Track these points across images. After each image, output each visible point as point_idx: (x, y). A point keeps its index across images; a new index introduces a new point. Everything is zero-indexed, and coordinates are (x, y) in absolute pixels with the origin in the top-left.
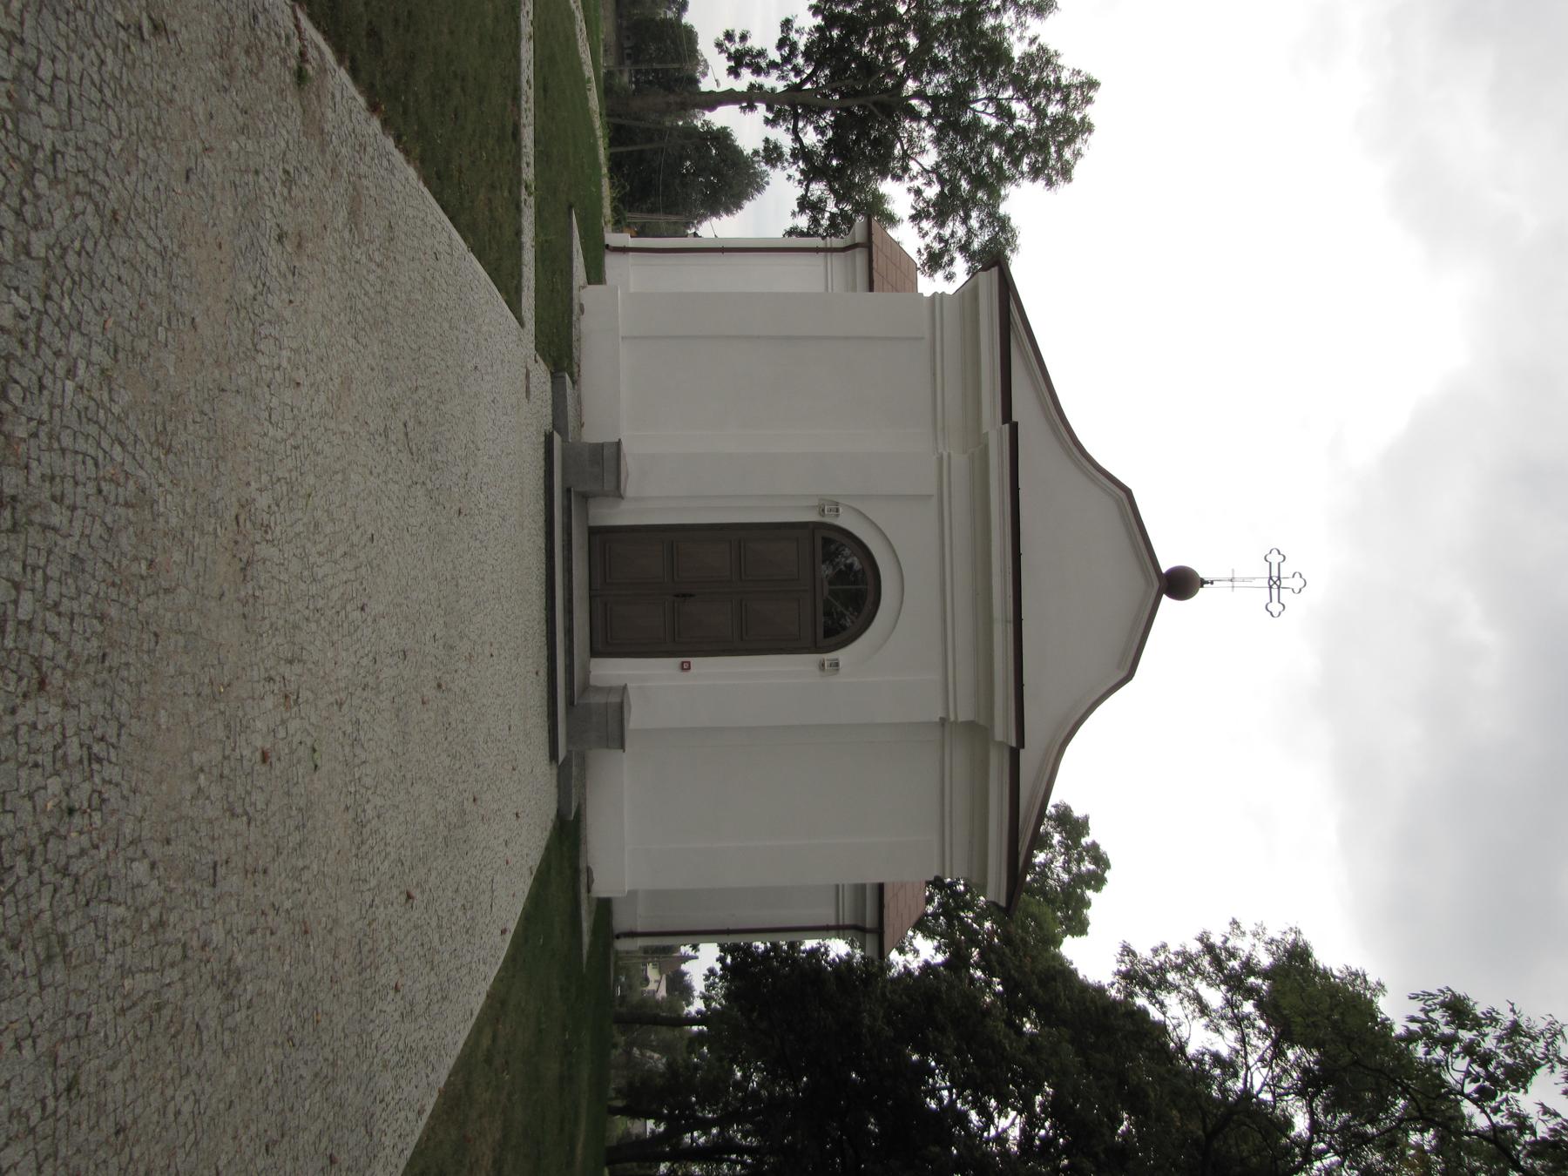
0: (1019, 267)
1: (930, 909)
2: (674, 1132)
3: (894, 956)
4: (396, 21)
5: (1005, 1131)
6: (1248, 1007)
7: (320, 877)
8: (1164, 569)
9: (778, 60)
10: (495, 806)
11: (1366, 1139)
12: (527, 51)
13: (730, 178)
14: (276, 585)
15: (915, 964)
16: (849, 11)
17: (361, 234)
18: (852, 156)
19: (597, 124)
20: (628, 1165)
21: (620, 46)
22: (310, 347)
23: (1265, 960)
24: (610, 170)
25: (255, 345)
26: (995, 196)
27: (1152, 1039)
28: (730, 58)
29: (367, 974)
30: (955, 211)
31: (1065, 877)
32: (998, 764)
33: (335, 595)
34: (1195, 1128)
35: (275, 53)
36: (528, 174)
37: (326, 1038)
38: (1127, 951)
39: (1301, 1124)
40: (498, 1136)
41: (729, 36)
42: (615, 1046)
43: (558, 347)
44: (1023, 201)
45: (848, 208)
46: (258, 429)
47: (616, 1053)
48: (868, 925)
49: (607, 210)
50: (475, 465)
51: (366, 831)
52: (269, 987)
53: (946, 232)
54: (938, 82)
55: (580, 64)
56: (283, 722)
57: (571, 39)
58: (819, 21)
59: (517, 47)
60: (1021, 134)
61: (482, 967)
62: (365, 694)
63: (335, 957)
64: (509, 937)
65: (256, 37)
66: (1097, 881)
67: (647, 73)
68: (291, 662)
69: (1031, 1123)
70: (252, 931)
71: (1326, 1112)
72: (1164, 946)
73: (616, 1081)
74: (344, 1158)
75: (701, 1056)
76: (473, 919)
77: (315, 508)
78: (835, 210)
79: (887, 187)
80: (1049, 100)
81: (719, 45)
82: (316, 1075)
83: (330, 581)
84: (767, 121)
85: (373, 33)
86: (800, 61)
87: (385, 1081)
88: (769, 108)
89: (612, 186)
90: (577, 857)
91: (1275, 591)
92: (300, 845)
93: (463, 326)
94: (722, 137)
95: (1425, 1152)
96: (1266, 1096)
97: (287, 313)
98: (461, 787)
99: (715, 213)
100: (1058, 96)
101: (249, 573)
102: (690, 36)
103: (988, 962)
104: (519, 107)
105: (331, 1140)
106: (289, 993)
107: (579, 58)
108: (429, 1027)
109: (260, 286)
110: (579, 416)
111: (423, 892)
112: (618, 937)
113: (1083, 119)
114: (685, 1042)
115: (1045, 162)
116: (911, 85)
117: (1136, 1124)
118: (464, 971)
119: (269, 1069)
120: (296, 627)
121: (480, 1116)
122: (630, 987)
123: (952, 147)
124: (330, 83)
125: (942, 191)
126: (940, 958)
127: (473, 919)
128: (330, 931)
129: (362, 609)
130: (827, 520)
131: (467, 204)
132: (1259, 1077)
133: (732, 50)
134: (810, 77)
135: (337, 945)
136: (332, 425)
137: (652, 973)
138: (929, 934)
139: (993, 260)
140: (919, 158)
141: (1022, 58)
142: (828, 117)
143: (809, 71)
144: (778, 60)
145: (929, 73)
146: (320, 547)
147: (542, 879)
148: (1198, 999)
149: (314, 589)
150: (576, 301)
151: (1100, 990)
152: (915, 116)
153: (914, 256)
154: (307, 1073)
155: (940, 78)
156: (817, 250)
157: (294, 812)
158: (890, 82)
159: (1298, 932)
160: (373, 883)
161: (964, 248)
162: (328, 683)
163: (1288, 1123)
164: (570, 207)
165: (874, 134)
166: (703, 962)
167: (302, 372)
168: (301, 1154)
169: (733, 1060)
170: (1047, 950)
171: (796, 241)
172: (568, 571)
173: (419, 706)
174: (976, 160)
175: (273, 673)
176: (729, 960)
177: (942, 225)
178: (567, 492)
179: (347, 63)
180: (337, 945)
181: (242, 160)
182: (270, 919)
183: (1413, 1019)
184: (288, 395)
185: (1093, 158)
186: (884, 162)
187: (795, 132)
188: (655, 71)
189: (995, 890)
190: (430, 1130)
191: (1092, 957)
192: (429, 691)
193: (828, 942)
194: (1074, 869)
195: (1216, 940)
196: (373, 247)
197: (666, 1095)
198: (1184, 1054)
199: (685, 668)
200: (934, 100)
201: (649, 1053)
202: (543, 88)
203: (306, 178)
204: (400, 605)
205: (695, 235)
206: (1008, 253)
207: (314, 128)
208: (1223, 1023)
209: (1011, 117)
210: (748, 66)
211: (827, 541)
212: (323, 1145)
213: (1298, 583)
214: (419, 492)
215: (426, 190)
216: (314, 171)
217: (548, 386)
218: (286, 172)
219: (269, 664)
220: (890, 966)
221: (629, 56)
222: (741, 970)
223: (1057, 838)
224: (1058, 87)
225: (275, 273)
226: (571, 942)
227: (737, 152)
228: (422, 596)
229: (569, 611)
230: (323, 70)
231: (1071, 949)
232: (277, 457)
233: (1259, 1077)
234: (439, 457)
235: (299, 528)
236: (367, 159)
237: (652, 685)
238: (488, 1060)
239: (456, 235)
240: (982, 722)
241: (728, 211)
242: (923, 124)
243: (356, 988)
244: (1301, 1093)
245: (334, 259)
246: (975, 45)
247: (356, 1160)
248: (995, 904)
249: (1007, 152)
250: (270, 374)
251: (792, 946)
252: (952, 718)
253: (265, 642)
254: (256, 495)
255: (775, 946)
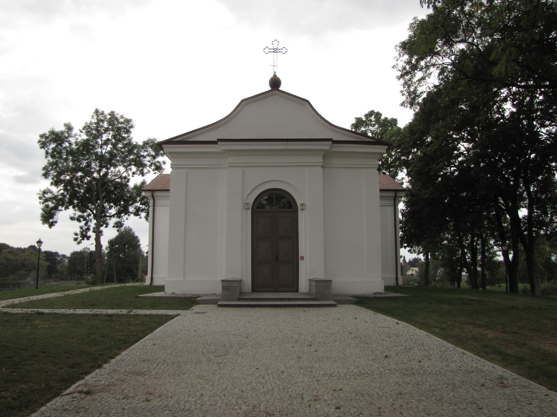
0: (161, 138)
1: (388, 174)
2: (467, 265)
3: (404, 186)
4: (68, 358)
5: (465, 148)
6: (423, 63)
7: (381, 388)
8: (270, 89)
9: (85, 222)
10: (353, 326)
11: (469, 23)
12: (80, 311)
13: (127, 240)
14: (275, 403)
15: (407, 179)
16: (68, 196)
17: (146, 371)
18: (122, 197)
19: (106, 287)
20: (478, 282)
21: (78, 279)
22: (188, 390)
23: (406, 57)
24: (123, 283)
25: (187, 410)
26: (136, 146)
27: (433, 97)
28: (83, 239)
29: (415, 372)
30: (140, 161)
31: (377, 126)
32: (338, 148)
33: (278, 382)
34: (464, 82)
35: (79, 402)
36: (124, 311)
37: (439, 387)
38: (403, 104)
39: (462, 46)
40: (471, 326)
41: (76, 239)
42: (435, 286)
43: (187, 302)
44: (138, 136)
45: (138, 199)
46: (218, 409)
47: (438, 285)
48: (394, 195)
49: (137, 284)
50: (230, 332)
51: (363, 372)
52: (421, 407)
53: (148, 164)
54: (95, 165)
55: (84, 293)
56: (325, 401)
57: (75, 296)
58: (71, 207)
59: (78, 315)
60: (114, 137)
61: (411, 331)
62: (314, 372)
63: (409, 383)
64: (399, 322)
65: (73, 409)
66: (378, 115)
67: (88, 270)
68: (303, 398)
69: (462, 139)
70: (401, 413)
71: (457, 37)
72: (401, 92)
73: (448, 285)
74: (482, 381)
75: (439, 255)
76: (393, 334)
77: (247, 389)
78: (139, 203)
79: (131, 184)
80: (102, 126)
81: (79, 243)
82: (452, 391)
83: (273, 384)
84: (107, 227)
85: (72, 366)
86: (85, 214)
87: (453, 366)
88: (102, 226)
89: (129, 282)
90: (370, 297)
91: (278, 51)
92: (369, 396)
93: (180, 335)
94: (112, 243)
95: (472, 4)
96: (453, 58)
97: (176, 398)
98: (346, 338)
99: (139, 246)
100: (101, 123)
101: (271, 413)
102: (75, 254)
103: (406, 153)
104: (100, 315)
105: (476, 386)
106: (423, 400)
107: (82, 293)
108: (433, 350)
109: (166, 408)
110: (211, 295)
111: (385, 352)
112: (398, 284)
113: (109, 115)
114: (434, 261)
115: (124, 128)
116: (95, 175)
117: (463, 102)
118: (412, 338)
119: (451, 408)
120: (290, 396)
121: (464, 332)
122: (414, 280)
123: (118, 161)
124: (90, 382)
125: (134, 165)
126: (405, 170)
127: (393, 334)
128: (400, 385)
129: (283, 372)
130: (251, 207)
131: (135, 333)
132: (447, 60)
133: (81, 238)
134: (91, 211)
135: (405, 383)
136: (216, 383)
137: (409, 272)
138: (396, 174)
139: (159, 147)
140: (122, 173)
141: (87, 135)
142: (106, 205)
143: (89, 211)
144: (85, 222)
145: (91, 168)
146: (261, 387)
147: (378, 310)
148: (420, 80)
149: (277, 390)
150: (171, 296)
151: (416, 115)
152: (106, 174)
153: (157, 175)
154: (452, 394)
155: (93, 165)
156: (154, 209)
157: (358, 398)
158: (94, 183)
159: (396, 46)
160: (382, 369)
161: (154, 158)
162: (310, 385)
163: (462, 50)
164: (137, 297)
165: (112, 189)
166: (407, 254)
167: (197, 393)
168: (482, 396)
169: (441, 244)
170: (402, 132)
171: (150, 218)
172: (268, 299)
173: (317, 353)
174: (123, 153)
175: (307, 405)
176: (406, 245)
177: (146, 165)
178: (239, 299)
179: (83, 376)
180: (405, 383)
181: (119, 415)
182: (397, 407)
183: (428, 7)
184: (206, 398)
185: (123, 111)
186: (122, 185)
187: (110, 217)
188: (87, 266)
189: (382, 149)
190: (470, 350)
191: (405, 117)
192: (312, 349)
193: (399, 209)
194: (374, 123)
195: (399, 74)
196: (151, 367)
197: (453, 268)
198: (438, 86)
199: (303, 258)
200: (101, 167)
201: (438, 274)
202: (93, 306)
203: (126, 391)
204: (281, 359)
205: (147, 253)
206: (156, 142)
207: (107, 388)
208: (428, 72)
209: (108, 140)
210: (86, 233)
211: (258, 208)
212: (478, 388)
213: (276, 43)
214: (240, 352)
215: (130, 348)
216: (123, 388)
217: (201, 306)
218: (123, 398)
219: (304, 406)
220: (408, 188)
221: (81, 276)
222: (410, 240)
223: (363, 129)
224: (98, 123)
225: (161, 403)
226: (399, 300)
227: (117, 238)
228: (278, 351)
229: (282, 299)
230: (86, 385)
231: (402, 124)
232: (229, 403)
233: (447, 60)
234: (227, 344)
235: (254, 395)
236: (119, 369)
237: (309, 270)
238: (444, 329)
239: (147, 337)
240: (323, 153)
241: (138, 241)
242: (110, 171)
243: (420, 376)
244: (451, 46)
245: (155, 381)
246: (82, 152)
247: (482, 377)
248: (387, 150)
249: (120, 142)
250: (198, 405)
251: (401, 222)
252: (322, 164)
253: (295, 407)
254: (242, 411)
255: (401, 228)
